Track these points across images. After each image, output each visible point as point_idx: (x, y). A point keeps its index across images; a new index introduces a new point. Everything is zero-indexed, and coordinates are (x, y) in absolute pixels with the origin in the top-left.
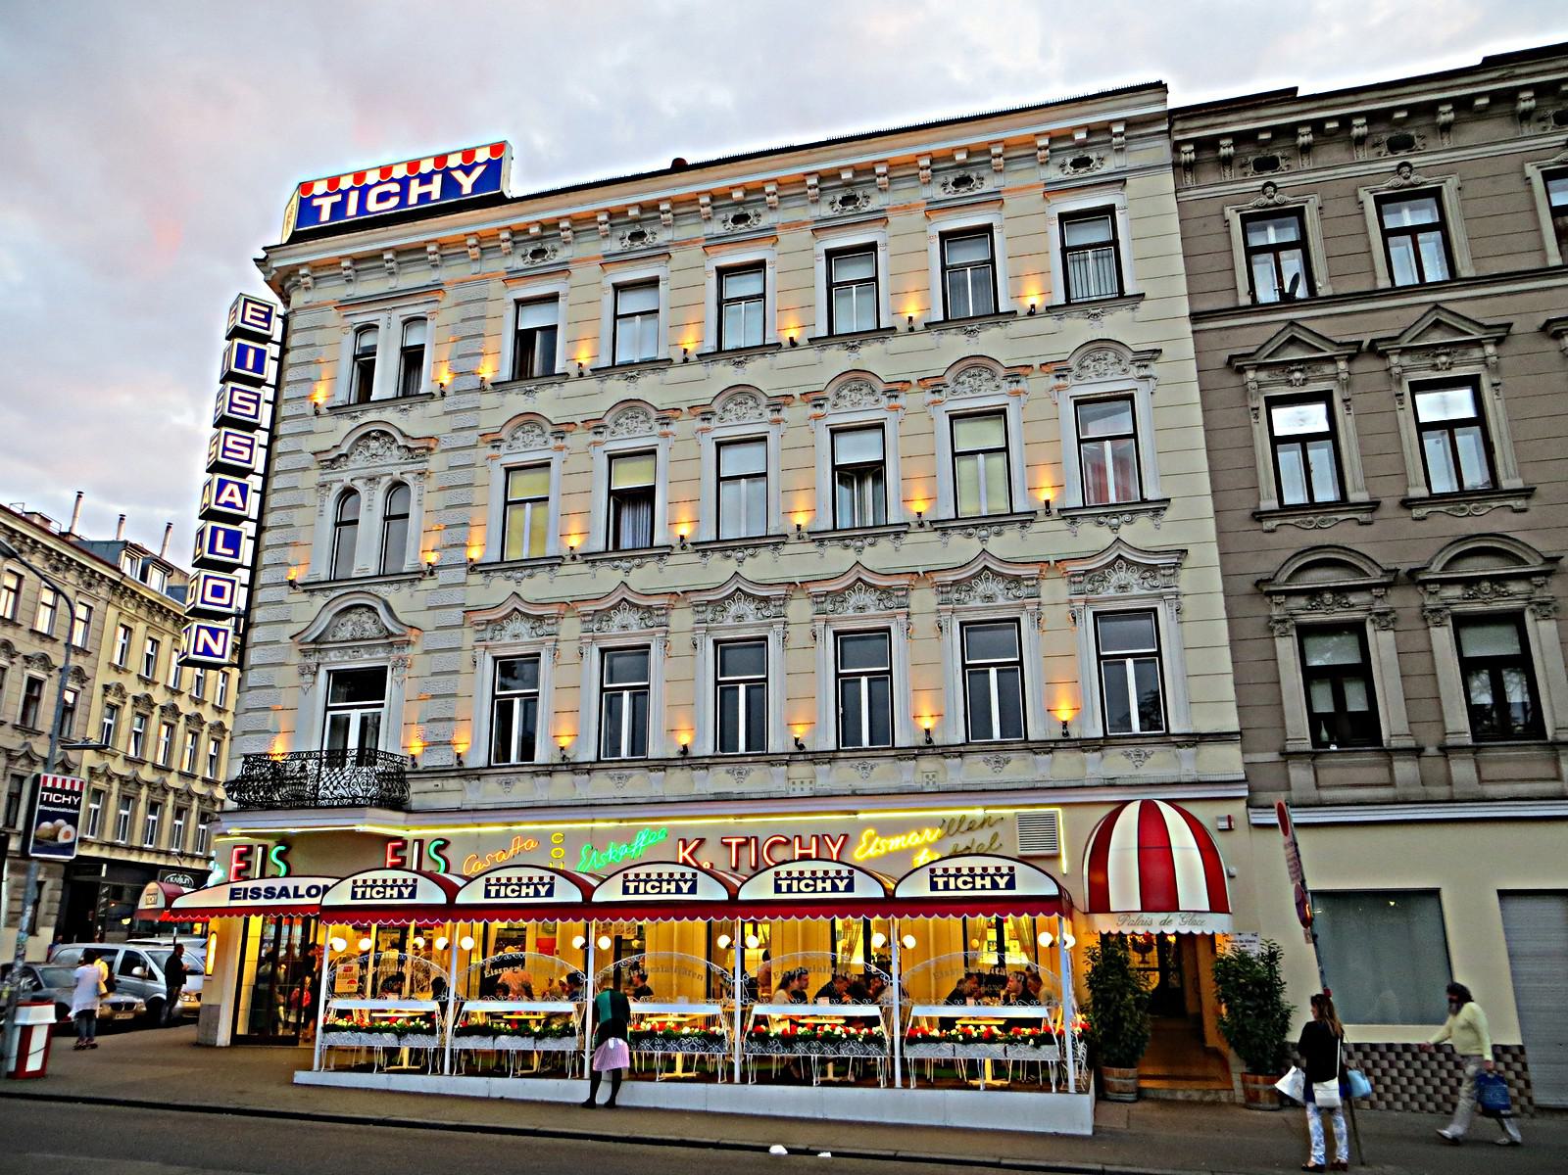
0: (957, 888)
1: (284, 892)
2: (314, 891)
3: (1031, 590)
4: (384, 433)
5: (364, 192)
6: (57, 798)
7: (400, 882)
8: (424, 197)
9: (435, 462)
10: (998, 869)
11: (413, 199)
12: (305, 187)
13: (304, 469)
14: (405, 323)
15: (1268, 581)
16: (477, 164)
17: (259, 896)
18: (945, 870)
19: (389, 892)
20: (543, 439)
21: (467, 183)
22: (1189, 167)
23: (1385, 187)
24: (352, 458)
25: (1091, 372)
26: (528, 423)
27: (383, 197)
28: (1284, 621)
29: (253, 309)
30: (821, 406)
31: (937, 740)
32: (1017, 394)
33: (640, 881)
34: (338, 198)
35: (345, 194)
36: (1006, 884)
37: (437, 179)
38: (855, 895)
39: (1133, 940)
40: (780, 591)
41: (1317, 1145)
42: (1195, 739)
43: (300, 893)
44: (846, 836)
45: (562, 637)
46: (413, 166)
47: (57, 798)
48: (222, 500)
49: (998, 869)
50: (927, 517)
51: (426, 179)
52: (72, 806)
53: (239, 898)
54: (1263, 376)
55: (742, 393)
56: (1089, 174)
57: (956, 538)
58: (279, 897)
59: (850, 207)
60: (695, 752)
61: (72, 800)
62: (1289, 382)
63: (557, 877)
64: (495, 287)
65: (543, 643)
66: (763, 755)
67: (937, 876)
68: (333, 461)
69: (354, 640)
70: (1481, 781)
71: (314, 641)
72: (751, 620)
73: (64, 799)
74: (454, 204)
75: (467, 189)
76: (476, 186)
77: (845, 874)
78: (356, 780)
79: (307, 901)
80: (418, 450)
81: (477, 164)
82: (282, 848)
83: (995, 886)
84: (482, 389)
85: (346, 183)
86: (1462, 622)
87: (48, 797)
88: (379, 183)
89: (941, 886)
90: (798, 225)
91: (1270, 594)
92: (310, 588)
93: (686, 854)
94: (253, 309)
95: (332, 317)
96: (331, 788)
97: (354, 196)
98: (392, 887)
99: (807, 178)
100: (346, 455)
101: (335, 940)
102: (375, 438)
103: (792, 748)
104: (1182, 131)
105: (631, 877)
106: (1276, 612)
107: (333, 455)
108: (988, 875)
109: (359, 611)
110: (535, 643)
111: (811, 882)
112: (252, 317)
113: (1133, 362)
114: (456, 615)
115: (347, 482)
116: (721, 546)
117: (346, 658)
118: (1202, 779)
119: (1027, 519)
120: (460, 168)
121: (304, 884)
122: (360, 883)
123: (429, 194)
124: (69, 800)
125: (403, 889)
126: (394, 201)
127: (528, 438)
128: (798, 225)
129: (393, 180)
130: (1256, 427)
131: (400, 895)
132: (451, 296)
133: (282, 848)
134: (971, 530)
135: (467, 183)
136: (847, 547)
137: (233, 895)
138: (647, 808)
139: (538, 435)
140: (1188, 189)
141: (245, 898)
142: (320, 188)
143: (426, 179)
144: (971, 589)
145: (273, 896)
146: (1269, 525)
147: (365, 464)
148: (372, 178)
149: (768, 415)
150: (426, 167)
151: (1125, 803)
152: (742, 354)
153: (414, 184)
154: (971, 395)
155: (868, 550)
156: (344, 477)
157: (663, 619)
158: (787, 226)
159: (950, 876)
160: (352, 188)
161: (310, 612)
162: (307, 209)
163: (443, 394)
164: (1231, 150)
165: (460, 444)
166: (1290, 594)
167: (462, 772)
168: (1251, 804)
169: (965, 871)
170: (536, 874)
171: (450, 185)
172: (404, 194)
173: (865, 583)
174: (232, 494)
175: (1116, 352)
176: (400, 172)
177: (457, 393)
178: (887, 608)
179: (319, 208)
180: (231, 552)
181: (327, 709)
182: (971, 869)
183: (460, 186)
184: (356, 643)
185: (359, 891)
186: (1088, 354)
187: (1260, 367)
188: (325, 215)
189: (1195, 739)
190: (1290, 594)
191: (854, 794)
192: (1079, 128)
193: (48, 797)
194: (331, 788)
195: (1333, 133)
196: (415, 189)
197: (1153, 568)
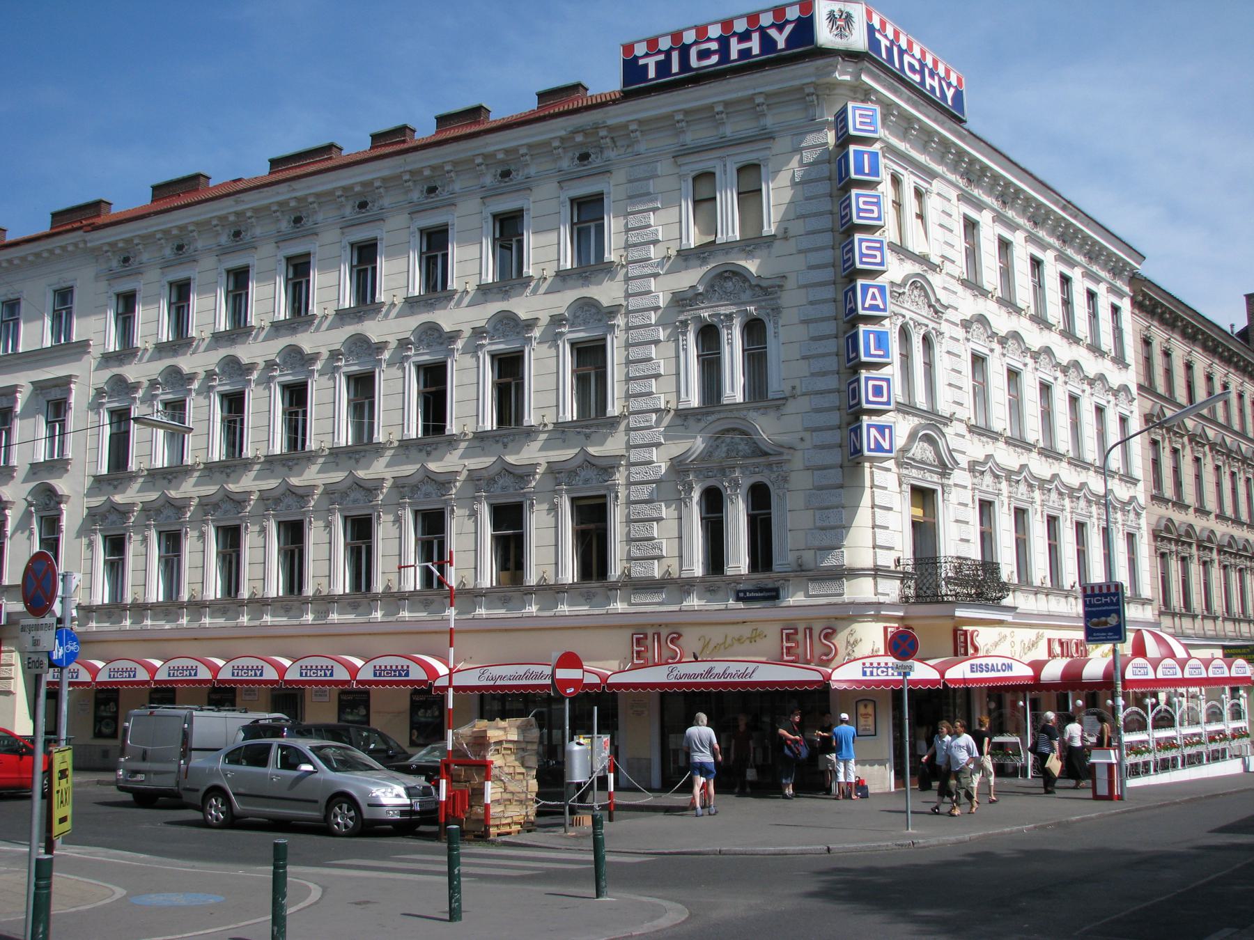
0: (878, 675)
5: (684, 51)
6: (1098, 600)
7: (324, 667)
8: (745, 53)
11: (734, 55)
12: (628, 48)
16: (788, 22)
21: (781, 39)
27: (703, 55)
29: (861, 116)
35: (668, 53)
37: (756, 37)
46: (727, 24)
47: (1098, 600)
48: (866, 305)
52: (1112, 603)
61: (1111, 600)
73: (1104, 600)
74: (772, 59)
75: (781, 45)
81: (788, 22)
85: (665, 44)
87: (1090, 601)
88: (696, 43)
94: (861, 116)
96: (925, 589)
97: (675, 56)
98: (251, 670)
99: (575, 135)
111: (885, 670)
112: (862, 123)
120: (772, 26)
122: (868, 665)
123: (750, 49)
124: (1108, 600)
126: (715, 59)
129: (710, 40)
135: (781, 39)
142: (640, 50)
143: (745, 37)
148: (689, 37)
160: (671, 49)
162: (632, 69)
169: (883, 665)
171: (768, 44)
174: (874, 297)
179: (646, 66)
180: (881, 353)
182: (886, 664)
183: (774, 43)
185: (304, 672)
188: (652, 74)
192: (248, 209)
193: (1090, 601)
194: (925, 589)
196: (735, 47)
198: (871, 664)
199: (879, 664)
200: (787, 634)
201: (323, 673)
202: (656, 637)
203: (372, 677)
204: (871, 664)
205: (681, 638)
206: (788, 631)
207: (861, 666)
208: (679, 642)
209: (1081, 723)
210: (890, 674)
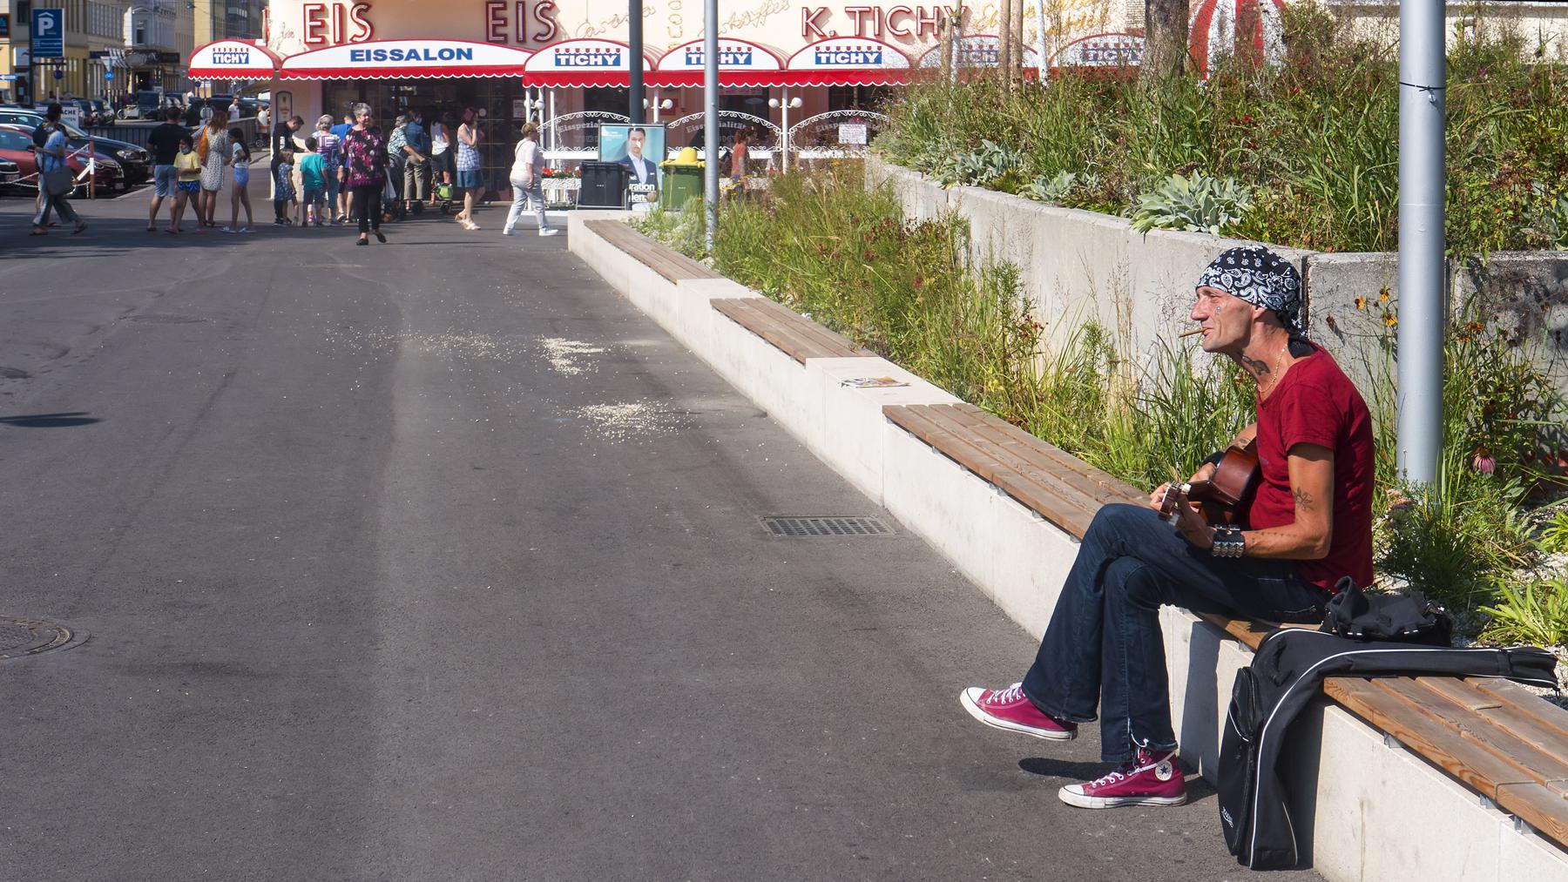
10: (608, 50)
17: (385, 58)
33: (570, 54)
36: (745, 60)
38: (883, 66)
39: (1215, 166)
41: (1382, 545)
43: (431, 55)
49: (608, 50)
53: (363, 60)
58: (407, 59)
63: (753, 48)
67: (821, 53)
77: (744, 50)
79: (440, 63)
83: (736, 61)
89: (563, 62)
101: (65, 67)
105: (693, 50)
108: (731, 53)
111: (229, 56)
121: (388, 47)
125: (241, 55)
141: (368, 59)
145: (401, 57)
159: (570, 54)
169: (583, 51)
170: (603, 47)
182: (588, 50)
198: (567, 50)
199: (577, 50)
200: (310, 11)
201: (861, 57)
202: (520, 7)
203: (552, 67)
204: (567, 50)
205: (371, 10)
206: (496, 6)
207: (815, 50)
208: (369, 15)
209: (487, 112)
210: (853, 61)
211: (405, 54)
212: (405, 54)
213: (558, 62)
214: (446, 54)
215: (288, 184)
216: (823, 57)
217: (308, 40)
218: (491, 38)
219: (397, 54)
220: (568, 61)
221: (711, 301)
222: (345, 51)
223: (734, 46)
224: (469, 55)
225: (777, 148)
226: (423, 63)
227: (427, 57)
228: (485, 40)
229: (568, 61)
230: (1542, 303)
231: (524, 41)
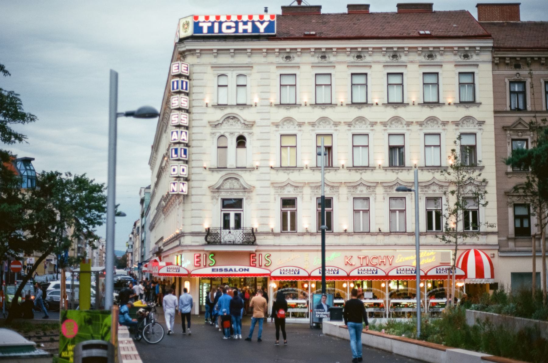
1: (231, 270)
2: (241, 270)
3: (300, 190)
4: (234, 117)
5: (221, 23)
9: (255, 130)
13: (205, 126)
14: (237, 76)
15: (508, 192)
17: (222, 271)
18: (440, 269)
19: (330, 272)
20: (294, 127)
21: (262, 28)
22: (497, 64)
23: (512, 79)
24: (223, 125)
25: (465, 125)
26: (288, 120)
27: (229, 27)
28: (511, 203)
30: (386, 126)
31: (382, 231)
32: (480, 129)
34: (210, 24)
35: (213, 23)
37: (250, 24)
40: (375, 185)
42: (486, 233)
43: (236, 270)
44: (352, 257)
45: (304, 193)
50: (418, 165)
51: (245, 23)
54: (511, 132)
55: (288, 120)
56: (361, 61)
57: (353, 172)
59: (395, 59)
60: (349, 231)
62: (518, 135)
64: (273, 68)
65: (298, 195)
66: (295, 232)
68: (216, 125)
69: (230, 189)
70: (515, 246)
71: (217, 189)
72: (437, 192)
76: (266, 30)
77: (336, 270)
78: (236, 235)
80: (250, 125)
81: (264, 21)
82: (213, 255)
83: (373, 273)
84: (271, 105)
86: (515, 206)
89: (439, 272)
90: (378, 62)
91: (508, 195)
92: (212, 170)
93: (348, 260)
95: (209, 69)
97: (216, 25)
100: (221, 124)
102: (232, 119)
103: (378, 231)
104: (496, 54)
106: (509, 200)
107: (217, 123)
109: (232, 179)
110: (295, 194)
113: (477, 124)
114: (268, 184)
115: (222, 133)
116: (355, 168)
117: (228, 195)
118: (488, 244)
119: (301, 169)
120: (258, 21)
127: (397, 125)
128: (378, 62)
130: (509, 147)
131: (177, 271)
132: (256, 68)
133: (213, 255)
134: (430, 170)
136: (357, 172)
137: (213, 270)
138: (369, 247)
139: (328, 124)
140: (496, 71)
144: (429, 188)
145: (227, 271)
146: (509, 176)
147: (228, 128)
149: (369, 127)
150: (245, 18)
151: (470, 250)
152: (289, 106)
153: (241, 24)
154: (359, 128)
155: (363, 173)
156: (222, 130)
157: (337, 190)
158: (375, 62)
161: (215, 178)
162: (197, 28)
163: (256, 106)
164: (509, 62)
165: (264, 124)
166: (513, 196)
167: (273, 233)
168: (499, 250)
170: (294, 268)
172: (237, 27)
173: (363, 184)
175: (473, 120)
176: (234, 18)
177: (261, 106)
178: (332, 192)
181: (221, 211)
184: (227, 190)
186: (465, 120)
187: (511, 130)
188: (205, 30)
189: (486, 233)
190: (513, 196)
191: (395, 245)
195: (536, 60)
197: (369, 187)
211: (229, 270)
212: (229, 270)
213: (437, 272)
214: (241, 270)
215: (185, 55)
216: (399, 272)
217: (196, 265)
218: (252, 265)
219: (226, 270)
220: (440, 272)
221: (484, 122)
222: (210, 269)
223: (330, 268)
224: (248, 270)
225: (385, 299)
226: (234, 273)
227: (235, 270)
228: (249, 265)
229: (440, 272)
230: (413, 336)
231: (261, 266)
